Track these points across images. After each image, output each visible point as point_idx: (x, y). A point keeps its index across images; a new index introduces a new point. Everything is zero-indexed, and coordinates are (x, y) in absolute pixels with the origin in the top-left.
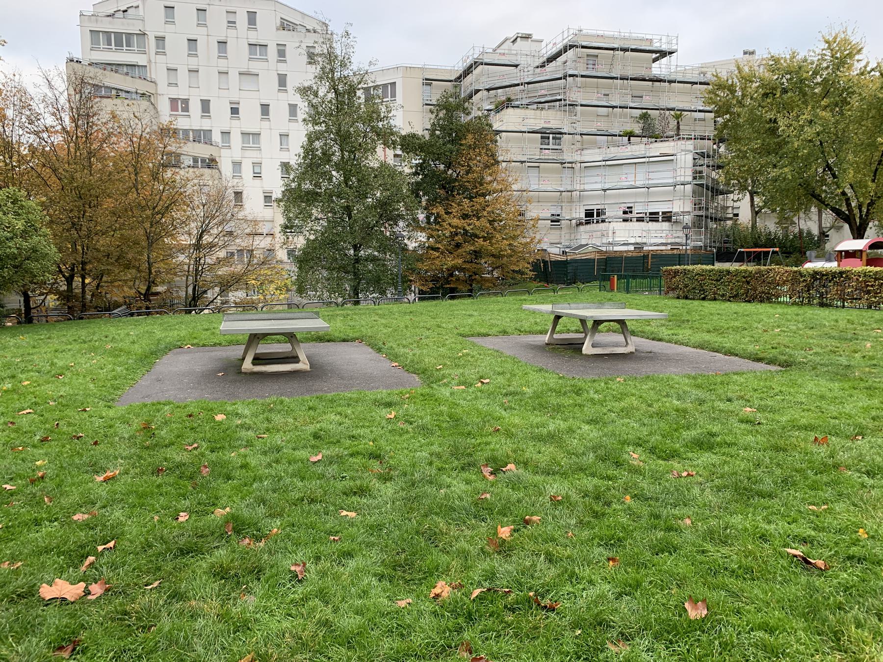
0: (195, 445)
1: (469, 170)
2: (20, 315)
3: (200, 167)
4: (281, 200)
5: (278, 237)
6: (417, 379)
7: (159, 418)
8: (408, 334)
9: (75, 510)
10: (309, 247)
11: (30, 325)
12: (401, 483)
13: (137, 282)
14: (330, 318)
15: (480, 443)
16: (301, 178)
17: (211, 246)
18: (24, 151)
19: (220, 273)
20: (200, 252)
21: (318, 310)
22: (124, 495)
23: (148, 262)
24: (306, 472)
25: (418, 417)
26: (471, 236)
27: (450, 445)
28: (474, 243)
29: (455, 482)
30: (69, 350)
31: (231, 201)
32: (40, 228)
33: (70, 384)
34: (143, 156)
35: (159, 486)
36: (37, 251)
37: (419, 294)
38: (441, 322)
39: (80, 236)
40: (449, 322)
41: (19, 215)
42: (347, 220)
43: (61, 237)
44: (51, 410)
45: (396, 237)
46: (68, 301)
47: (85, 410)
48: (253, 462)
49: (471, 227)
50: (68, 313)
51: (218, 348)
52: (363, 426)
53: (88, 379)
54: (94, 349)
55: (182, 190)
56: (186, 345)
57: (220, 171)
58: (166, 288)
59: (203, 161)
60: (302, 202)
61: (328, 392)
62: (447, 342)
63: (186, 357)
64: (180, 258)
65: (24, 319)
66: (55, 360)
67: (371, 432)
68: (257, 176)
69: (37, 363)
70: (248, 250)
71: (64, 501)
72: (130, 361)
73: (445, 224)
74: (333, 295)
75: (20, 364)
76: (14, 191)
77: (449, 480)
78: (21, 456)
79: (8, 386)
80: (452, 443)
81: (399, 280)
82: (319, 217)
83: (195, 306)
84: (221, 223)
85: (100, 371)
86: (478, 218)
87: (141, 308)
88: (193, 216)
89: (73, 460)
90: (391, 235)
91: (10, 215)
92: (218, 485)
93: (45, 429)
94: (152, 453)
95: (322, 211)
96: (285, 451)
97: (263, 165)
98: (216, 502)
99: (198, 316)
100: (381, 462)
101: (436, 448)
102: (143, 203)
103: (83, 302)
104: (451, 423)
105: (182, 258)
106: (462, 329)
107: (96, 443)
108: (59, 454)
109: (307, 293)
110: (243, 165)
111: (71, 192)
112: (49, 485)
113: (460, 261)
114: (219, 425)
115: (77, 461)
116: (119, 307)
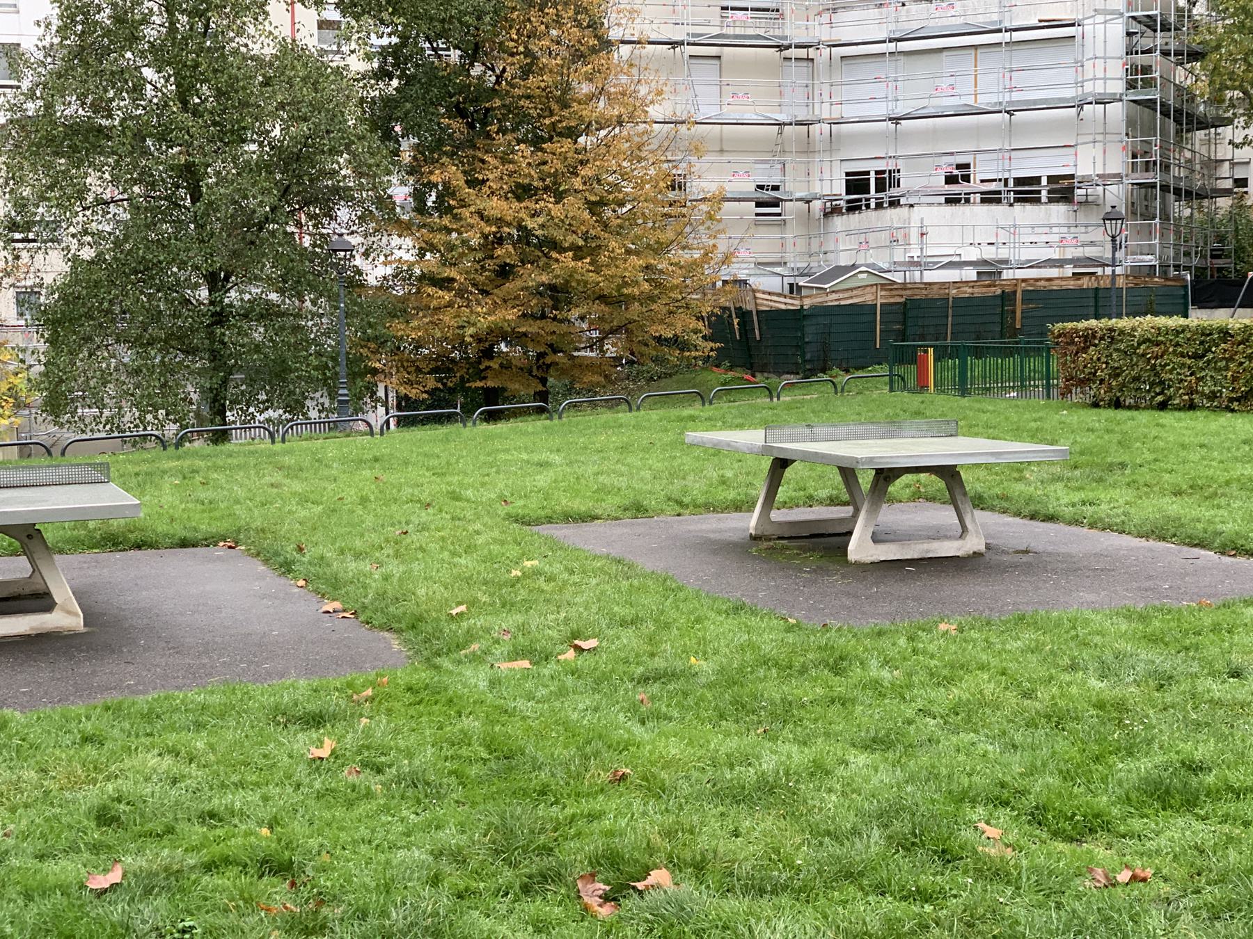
6: (396, 645)
8: (369, 521)
14: (140, 482)
15: (573, 816)
16: (54, 87)
21: (105, 458)
24: (77, 919)
25: (399, 750)
26: (540, 246)
27: (490, 824)
28: (548, 265)
38: (461, 484)
40: (483, 485)
42: (188, 203)
45: (330, 252)
49: (541, 220)
52: (241, 785)
62: (480, 540)
67: (265, 799)
73: (465, 213)
74: (149, 417)
80: (496, 820)
81: (342, 370)
82: (107, 196)
90: (314, 245)
95: (115, 181)
100: (293, 884)
101: (450, 836)
104: (492, 765)
113: (511, 315)
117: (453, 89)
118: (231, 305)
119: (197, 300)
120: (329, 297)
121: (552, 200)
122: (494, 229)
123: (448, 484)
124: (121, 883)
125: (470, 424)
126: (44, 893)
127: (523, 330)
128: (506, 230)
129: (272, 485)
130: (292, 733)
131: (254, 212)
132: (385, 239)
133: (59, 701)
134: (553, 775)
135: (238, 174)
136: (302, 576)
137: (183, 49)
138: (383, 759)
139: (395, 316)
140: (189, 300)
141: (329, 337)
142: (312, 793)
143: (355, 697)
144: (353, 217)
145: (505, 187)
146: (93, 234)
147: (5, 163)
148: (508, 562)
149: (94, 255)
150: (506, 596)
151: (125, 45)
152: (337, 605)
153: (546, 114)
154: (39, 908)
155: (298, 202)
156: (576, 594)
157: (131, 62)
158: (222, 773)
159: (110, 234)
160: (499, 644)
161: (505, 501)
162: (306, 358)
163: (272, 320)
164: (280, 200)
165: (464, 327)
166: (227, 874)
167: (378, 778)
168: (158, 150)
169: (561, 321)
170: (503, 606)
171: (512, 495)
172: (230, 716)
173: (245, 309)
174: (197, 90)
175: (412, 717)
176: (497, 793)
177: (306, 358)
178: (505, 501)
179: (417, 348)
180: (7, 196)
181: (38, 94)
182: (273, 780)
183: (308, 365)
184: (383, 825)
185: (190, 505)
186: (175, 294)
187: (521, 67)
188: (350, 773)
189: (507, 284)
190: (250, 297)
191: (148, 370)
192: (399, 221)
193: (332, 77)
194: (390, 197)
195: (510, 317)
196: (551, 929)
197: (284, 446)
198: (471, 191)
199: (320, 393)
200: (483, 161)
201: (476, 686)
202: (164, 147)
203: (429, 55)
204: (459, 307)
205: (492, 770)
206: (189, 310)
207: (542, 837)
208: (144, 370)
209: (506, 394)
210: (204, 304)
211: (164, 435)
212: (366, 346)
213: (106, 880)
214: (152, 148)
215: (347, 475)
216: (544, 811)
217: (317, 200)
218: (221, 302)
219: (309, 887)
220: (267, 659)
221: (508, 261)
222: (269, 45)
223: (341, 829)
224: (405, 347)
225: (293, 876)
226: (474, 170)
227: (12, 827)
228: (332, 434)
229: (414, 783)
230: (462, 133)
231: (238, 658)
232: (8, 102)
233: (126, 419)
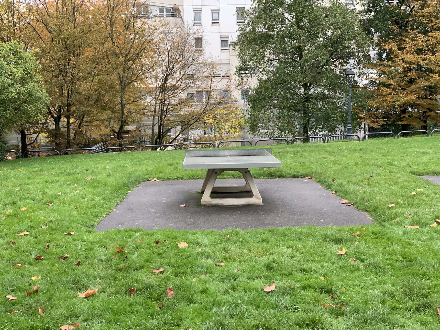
0: (162, 269)
1: (424, 4)
2: (18, 150)
3: (165, 16)
4: (236, 44)
5: (234, 78)
6: (368, 217)
7: (131, 243)
8: (358, 172)
9: (63, 321)
10: (261, 87)
11: (26, 159)
12: (353, 318)
13: (112, 122)
14: (281, 155)
15: (436, 285)
16: (255, 22)
17: (175, 88)
18: (23, 10)
19: (182, 113)
20: (165, 94)
21: (269, 147)
22: (102, 311)
23: (121, 104)
24: (261, 300)
25: (369, 254)
26: (426, 72)
27: (404, 284)
28: (429, 79)
29: (409, 323)
30: (57, 181)
31: (192, 47)
32: (35, 76)
33: (58, 211)
34: (117, 8)
35: (131, 305)
36: (32, 95)
37: (369, 131)
38: (393, 159)
39: (66, 82)
40: (401, 160)
41: (18, 64)
42: (298, 60)
43: (51, 82)
44: (43, 233)
45: (346, 75)
46: (56, 138)
47: (70, 234)
48: (212, 288)
49: (426, 62)
50: (56, 149)
51: (180, 181)
52: (314, 261)
53: (72, 207)
54: (77, 181)
55: (150, 38)
56: (153, 178)
57: (182, 20)
58: (136, 126)
59: (168, 10)
60: (256, 44)
61: (279, 226)
62: (400, 180)
63: (152, 190)
64: (147, 100)
65: (21, 154)
66: (47, 190)
67: (322, 267)
68: (215, 22)
69: (32, 192)
70: (207, 91)
71: (55, 313)
72: (107, 192)
73: (397, 60)
74: (283, 133)
75: (19, 193)
76: (15, 44)
77: (403, 320)
78: (20, 271)
79: (9, 211)
80: (406, 283)
81: (349, 117)
82: (272, 58)
83: (160, 143)
84: (183, 67)
85: (82, 200)
86: (434, 53)
87: (114, 144)
88: (159, 61)
89: (61, 278)
90: (341, 73)
91: (11, 65)
92: (181, 307)
93: (39, 249)
94: (125, 275)
95: (274, 53)
96: (241, 279)
97: (221, 12)
98: (180, 323)
99: (162, 152)
100: (332, 297)
101: (388, 287)
102: (118, 51)
103: (67, 139)
104: (404, 263)
105: (149, 100)
106: (416, 167)
107: (79, 264)
108: (50, 272)
109: (259, 131)
110: (203, 12)
111: (59, 43)
112: (42, 297)
113: (414, 97)
114: (182, 252)
115: (64, 279)
116: (96, 144)
117: (394, 14)
118: (311, 95)
119: (300, 93)
120: (345, 91)
121: (431, 54)
122: (408, 65)
123: (388, 159)
124: (275, 290)
125: (396, 137)
126: (250, 290)
127: (418, 103)
128: (413, 66)
129: (324, 158)
130: (331, 244)
131: (320, 62)
132: (366, 70)
133: (254, 227)
134: (428, 269)
135: (316, 49)
136: (334, 190)
137: (298, 6)
138: (364, 257)
139: (369, 98)
140: (297, 93)
141: (345, 106)
142: (338, 266)
143: (353, 234)
144: (355, 63)
145: (413, 50)
146: (267, 71)
147: (239, 48)
148: (411, 189)
149: (267, 78)
150: (410, 201)
151: (279, 6)
152: (347, 201)
153: (430, 22)
154: (248, 295)
155: (336, 58)
156: (437, 202)
157: (281, 12)
158: (308, 256)
159: (272, 71)
160: (407, 219)
161: (410, 166)
162: (336, 113)
163: (325, 100)
164: (330, 58)
165: (395, 102)
166: (310, 291)
167: (362, 263)
168: (289, 42)
169: (433, 100)
170: (409, 205)
171: (413, 164)
172: (310, 237)
173: (316, 96)
174: (303, 21)
175: (374, 243)
176: (406, 273)
177: (336, 113)
178: (410, 166)
179: (377, 109)
180: (240, 59)
181: (251, 24)
182: (325, 260)
183: (337, 116)
184: (364, 281)
185: (297, 164)
186: (292, 91)
187: (420, 5)
188: (352, 261)
189: (412, 86)
190: (318, 92)
191: (283, 117)
192: (372, 64)
193: (350, 13)
194: (369, 55)
195: (413, 98)
196: (427, 325)
197: (328, 144)
198: (400, 52)
199: (341, 125)
200: (405, 41)
201: (398, 234)
202: (291, 41)
203: (386, 3)
204: (394, 95)
205: (404, 265)
206: (297, 97)
207: (424, 291)
208: (282, 117)
209: (410, 127)
210: (302, 95)
211: (287, 139)
212: (358, 109)
213: (270, 288)
214: (287, 41)
215: (350, 155)
216: (424, 282)
217: (342, 57)
218: (308, 93)
219: (338, 299)
220: (322, 218)
221: (413, 77)
222: (328, 3)
223: (349, 280)
224: (372, 109)
225: (332, 295)
226: (401, 44)
227: (240, 267)
228: (345, 140)
229: (375, 267)
230: (397, 30)
231: (312, 217)
232: (241, 27)
233: (275, 134)
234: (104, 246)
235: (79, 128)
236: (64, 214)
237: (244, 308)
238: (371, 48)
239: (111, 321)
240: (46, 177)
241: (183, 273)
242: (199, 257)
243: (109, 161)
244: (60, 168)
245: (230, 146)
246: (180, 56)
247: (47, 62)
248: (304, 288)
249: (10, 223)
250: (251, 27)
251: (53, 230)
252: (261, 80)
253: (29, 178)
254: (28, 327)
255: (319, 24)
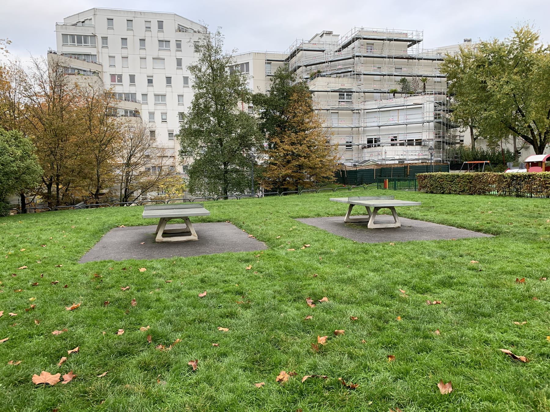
0: (128, 287)
2: (19, 208)
4: (179, 136)
6: (265, 245)
7: (105, 270)
10: (196, 164)
11: (25, 214)
12: (256, 309)
13: (91, 187)
14: (210, 208)
15: (305, 284)
16: (191, 122)
17: (136, 164)
19: (142, 181)
20: (129, 168)
21: (202, 203)
22: (84, 318)
24: (197, 303)
25: (266, 268)
26: (296, 156)
27: (286, 285)
28: (298, 160)
29: (290, 309)
32: (31, 155)
34: (94, 110)
35: (105, 313)
38: (279, 209)
39: (56, 159)
41: (19, 147)
44: (38, 266)
45: (250, 157)
46: (48, 199)
47: (59, 266)
48: (163, 297)
49: (297, 150)
50: (48, 207)
51: (141, 227)
52: (231, 275)
53: (61, 247)
54: (64, 229)
56: (121, 225)
57: (141, 118)
59: (131, 112)
60: (192, 136)
61: (209, 254)
62: (283, 222)
63: (121, 233)
64: (117, 172)
65: (21, 211)
66: (41, 236)
67: (237, 278)
68: (164, 121)
69: (30, 237)
71: (47, 323)
72: (87, 236)
73: (280, 149)
74: (211, 194)
76: (16, 132)
77: (286, 308)
79: (12, 252)
80: (288, 285)
81: (252, 184)
82: (203, 146)
84: (142, 150)
86: (301, 145)
88: (125, 146)
89: (52, 298)
90: (247, 156)
91: (13, 147)
92: (142, 312)
95: (204, 142)
96: (183, 290)
97: (168, 114)
98: (141, 322)
100: (243, 297)
101: (277, 288)
102: (95, 138)
103: (57, 199)
105: (118, 172)
107: (66, 287)
109: (195, 193)
111: (50, 132)
112: (37, 312)
113: (290, 171)
116: (79, 203)
152: (252, 235)
156: (305, 234)
167: (261, 274)
192: (265, 150)
223: (253, 285)
234: (85, 273)
235: (66, 192)
236: (55, 252)
237: (185, 309)
238: (264, 141)
239: (91, 325)
240: (41, 227)
241: (143, 289)
242: (154, 277)
243: (89, 215)
244: (51, 220)
245: (176, 203)
246: (139, 143)
247: (41, 145)
248: (225, 293)
249: (12, 260)
250: (188, 125)
251: (46, 264)
252: (196, 159)
253: (28, 228)
254: (26, 334)
255: (232, 125)
